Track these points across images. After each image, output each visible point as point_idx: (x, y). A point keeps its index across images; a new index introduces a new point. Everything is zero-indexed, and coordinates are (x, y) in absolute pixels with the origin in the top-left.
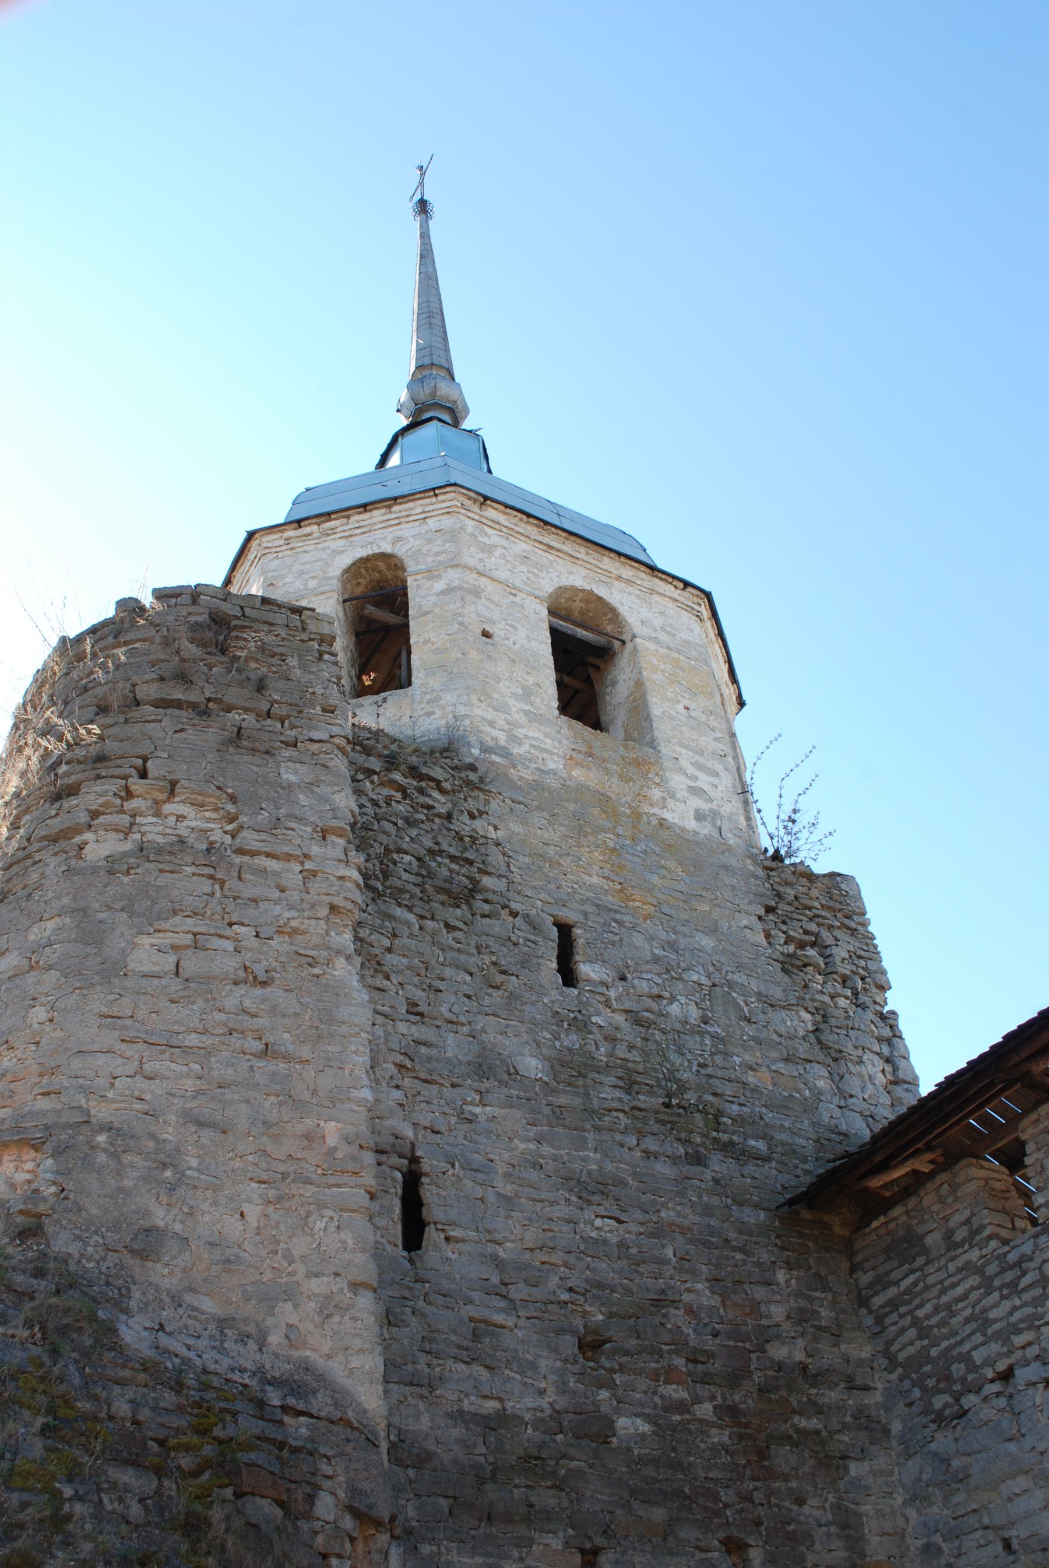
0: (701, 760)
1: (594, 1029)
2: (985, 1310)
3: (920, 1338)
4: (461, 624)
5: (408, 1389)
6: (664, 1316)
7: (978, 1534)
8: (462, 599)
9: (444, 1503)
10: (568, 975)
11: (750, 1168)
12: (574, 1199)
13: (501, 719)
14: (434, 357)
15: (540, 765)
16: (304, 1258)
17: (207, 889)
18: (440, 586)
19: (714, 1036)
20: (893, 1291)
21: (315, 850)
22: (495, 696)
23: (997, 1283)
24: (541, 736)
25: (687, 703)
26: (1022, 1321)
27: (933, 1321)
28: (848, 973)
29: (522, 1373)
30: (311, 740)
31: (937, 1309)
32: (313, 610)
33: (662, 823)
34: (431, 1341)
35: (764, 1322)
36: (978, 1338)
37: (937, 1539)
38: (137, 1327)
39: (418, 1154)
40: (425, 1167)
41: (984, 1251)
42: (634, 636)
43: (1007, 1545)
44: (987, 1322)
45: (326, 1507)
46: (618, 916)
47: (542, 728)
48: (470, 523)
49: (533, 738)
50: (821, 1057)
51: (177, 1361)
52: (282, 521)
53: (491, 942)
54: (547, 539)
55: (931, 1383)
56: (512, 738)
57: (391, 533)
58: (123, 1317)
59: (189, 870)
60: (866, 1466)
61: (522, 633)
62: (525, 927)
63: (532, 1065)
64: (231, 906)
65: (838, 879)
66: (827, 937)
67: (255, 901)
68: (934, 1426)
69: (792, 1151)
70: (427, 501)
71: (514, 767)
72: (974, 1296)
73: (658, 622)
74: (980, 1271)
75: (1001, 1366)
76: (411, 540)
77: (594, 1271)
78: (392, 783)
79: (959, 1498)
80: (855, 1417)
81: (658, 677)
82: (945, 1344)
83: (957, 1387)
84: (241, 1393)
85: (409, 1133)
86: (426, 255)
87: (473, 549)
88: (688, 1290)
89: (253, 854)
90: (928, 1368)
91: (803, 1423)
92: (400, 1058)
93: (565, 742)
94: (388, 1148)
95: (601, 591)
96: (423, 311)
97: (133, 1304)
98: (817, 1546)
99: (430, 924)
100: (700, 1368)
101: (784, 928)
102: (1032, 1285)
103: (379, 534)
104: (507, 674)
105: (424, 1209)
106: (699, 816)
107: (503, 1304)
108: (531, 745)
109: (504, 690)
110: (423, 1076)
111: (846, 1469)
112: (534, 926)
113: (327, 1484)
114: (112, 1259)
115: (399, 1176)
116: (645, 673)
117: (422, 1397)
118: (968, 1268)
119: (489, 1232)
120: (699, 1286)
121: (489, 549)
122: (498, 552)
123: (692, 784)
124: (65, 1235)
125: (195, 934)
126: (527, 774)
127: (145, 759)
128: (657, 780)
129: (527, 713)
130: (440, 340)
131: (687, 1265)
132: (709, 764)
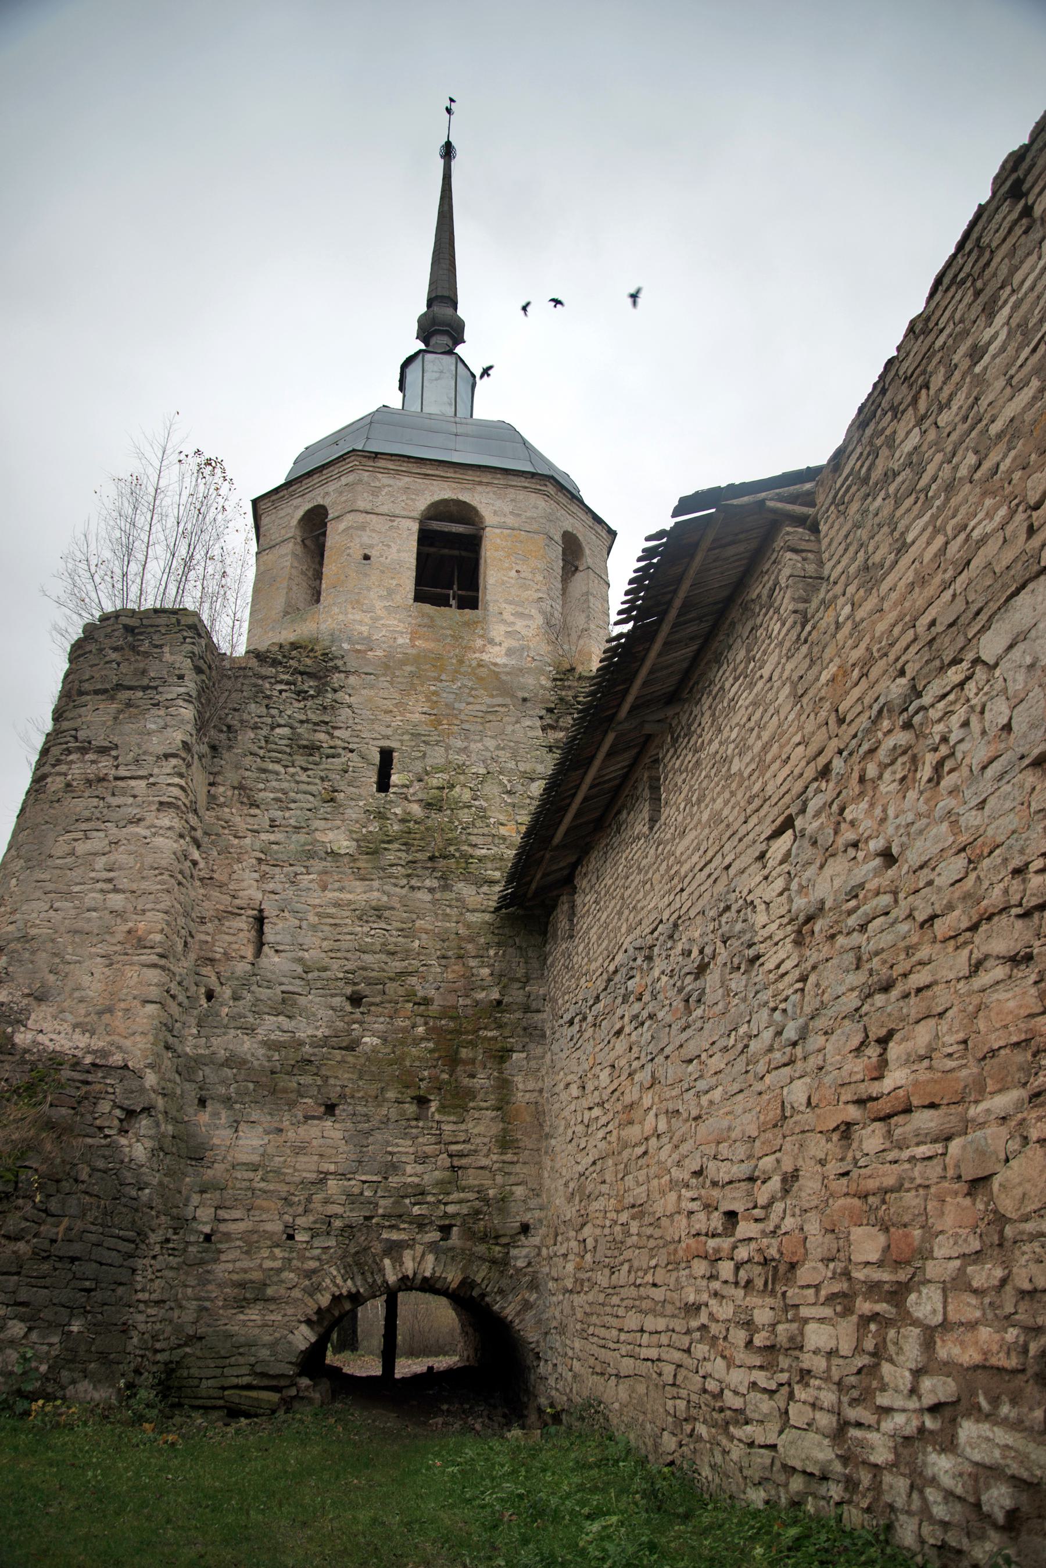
0: (520, 610)
9: (251, 1086)
10: (383, 785)
18: (342, 526)
21: (156, 771)
25: (518, 568)
29: (307, 1018)
40: (266, 914)
45: (105, 1106)
52: (283, 481)
64: (105, 811)
71: (371, 650)
95: (465, 497)
98: (478, 1098)
99: (291, 770)
100: (422, 1007)
103: (316, 492)
106: (510, 652)
132: (527, 612)
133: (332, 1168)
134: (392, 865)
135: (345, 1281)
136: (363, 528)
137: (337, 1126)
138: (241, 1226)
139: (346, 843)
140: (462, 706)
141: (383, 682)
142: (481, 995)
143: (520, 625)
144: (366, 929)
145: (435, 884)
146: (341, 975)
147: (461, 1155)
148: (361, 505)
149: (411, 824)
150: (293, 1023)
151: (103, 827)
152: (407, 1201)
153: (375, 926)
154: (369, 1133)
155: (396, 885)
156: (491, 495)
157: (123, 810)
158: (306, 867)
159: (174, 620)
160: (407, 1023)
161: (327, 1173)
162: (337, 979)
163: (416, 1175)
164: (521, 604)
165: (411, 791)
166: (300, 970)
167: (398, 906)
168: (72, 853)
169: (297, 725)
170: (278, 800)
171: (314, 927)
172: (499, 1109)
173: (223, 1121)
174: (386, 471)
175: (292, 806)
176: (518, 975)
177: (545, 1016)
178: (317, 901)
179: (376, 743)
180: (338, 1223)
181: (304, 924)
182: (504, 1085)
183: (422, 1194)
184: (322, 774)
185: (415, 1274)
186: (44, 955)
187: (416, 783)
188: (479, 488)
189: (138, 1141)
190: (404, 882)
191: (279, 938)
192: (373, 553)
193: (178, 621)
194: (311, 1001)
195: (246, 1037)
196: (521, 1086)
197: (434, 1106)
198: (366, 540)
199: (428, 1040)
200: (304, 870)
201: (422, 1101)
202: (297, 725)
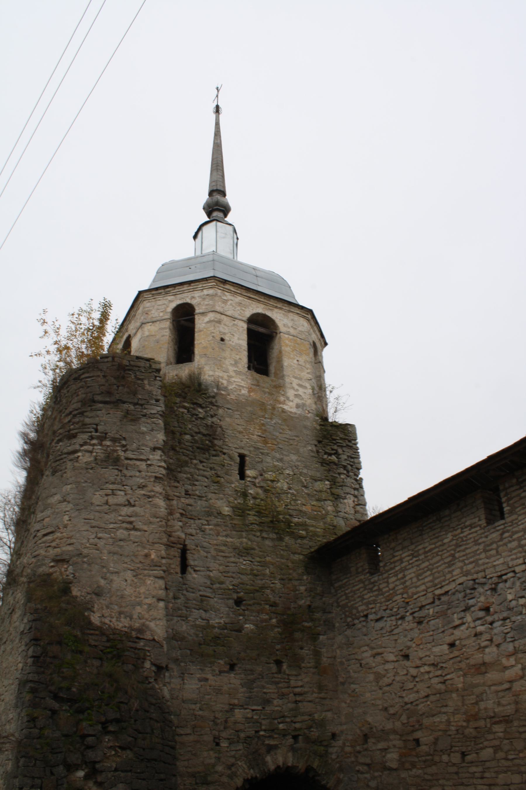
0: (301, 383)
1: (249, 495)
2: (363, 595)
3: (346, 599)
4: (213, 337)
5: (179, 619)
6: (263, 592)
7: (353, 661)
8: (214, 326)
10: (242, 475)
11: (299, 541)
12: (237, 555)
13: (225, 375)
14: (218, 186)
15: (238, 393)
16: (144, 593)
17: (117, 473)
18: (207, 319)
19: (292, 494)
20: (340, 583)
21: (151, 457)
22: (224, 366)
23: (367, 587)
24: (240, 380)
25: (298, 359)
26: (372, 601)
27: (350, 595)
28: (346, 464)
29: (215, 612)
30: (151, 414)
31: (351, 591)
32: (153, 359)
33: (284, 411)
34: (187, 603)
35: (297, 592)
36: (360, 603)
37: (344, 660)
38: (96, 617)
39: (186, 543)
40: (188, 547)
41: (366, 577)
42: (280, 332)
43: (361, 664)
44: (364, 599)
45: (147, 665)
46: (261, 451)
47: (241, 377)
48: (220, 291)
49: (237, 382)
50: (331, 498)
51: (107, 626)
53: (215, 466)
54: (249, 295)
55: (347, 613)
56: (229, 382)
57: (190, 295)
58: (92, 613)
59: (111, 467)
60: (325, 637)
61: (236, 336)
62: (228, 459)
63: (226, 510)
64: (123, 478)
65: (349, 426)
66: (340, 451)
67: (131, 476)
68: (346, 627)
69: (315, 534)
70: (204, 282)
71: (229, 395)
72: (361, 590)
73: (290, 324)
74: (363, 582)
75: (365, 613)
76: (197, 298)
77: (241, 579)
78: (185, 407)
79: (350, 649)
80: (324, 622)
81: (288, 349)
82: (352, 603)
83: (354, 617)
84: (125, 634)
85: (183, 536)
86: (217, 124)
87: (220, 303)
88: (273, 583)
89: (131, 459)
90: (347, 609)
91: (306, 624)
92: (181, 511)
93: (249, 381)
94: (176, 542)
95: (269, 314)
96: (214, 163)
97: (95, 609)
98: (306, 662)
100: (274, 608)
101: (324, 449)
102: (376, 590)
103: (185, 295)
104: (229, 356)
105: (187, 562)
106: (298, 406)
107: (211, 591)
108: (236, 385)
109: (228, 362)
110: (189, 516)
111: (319, 638)
112: (231, 458)
113: (148, 658)
114: (89, 596)
115: (179, 551)
116: (283, 348)
117: (184, 620)
118: (361, 581)
119: (208, 568)
120: (277, 582)
121: (225, 302)
122: (230, 302)
123: (296, 393)
124: (76, 589)
125: (112, 490)
126: (233, 397)
127: (97, 425)
128: (283, 393)
129: (235, 371)
130: (221, 177)
131: (273, 575)
132: (303, 384)
133: (236, 702)
134: (252, 524)
135: (249, 770)
136: (219, 322)
137: (237, 677)
138: (191, 738)
139: (227, 509)
140: (277, 434)
141: (237, 415)
142: (301, 602)
143: (301, 391)
144: (241, 560)
145: (275, 536)
146: (231, 587)
147: (300, 694)
148: (218, 309)
149: (259, 500)
150: (208, 615)
151: (123, 488)
152: (276, 721)
153: (246, 559)
154: (253, 681)
155: (255, 536)
156: (282, 315)
157: (134, 479)
158: (207, 521)
159: (148, 365)
160: (267, 617)
161: (234, 705)
162: (229, 589)
163: (279, 706)
164: (300, 379)
165: (257, 481)
166: (209, 583)
167: (257, 548)
168: (107, 503)
169: (194, 434)
170: (188, 479)
171: (214, 558)
172: (316, 667)
173: (175, 673)
174: (230, 291)
175: (196, 483)
176: (318, 592)
177: (333, 615)
178: (215, 542)
179: (237, 450)
180: (242, 735)
181: (209, 555)
182: (317, 654)
183: (283, 717)
184: (212, 466)
185: (283, 764)
186: (97, 567)
187: (259, 477)
188: (276, 310)
189: (165, 685)
190: (258, 534)
191: (196, 563)
192: (226, 338)
193: (150, 366)
194: (215, 601)
195: (183, 623)
196: (325, 655)
197: (285, 666)
198: (221, 329)
199: (278, 627)
200: (206, 522)
201: (279, 663)
202: (194, 434)
